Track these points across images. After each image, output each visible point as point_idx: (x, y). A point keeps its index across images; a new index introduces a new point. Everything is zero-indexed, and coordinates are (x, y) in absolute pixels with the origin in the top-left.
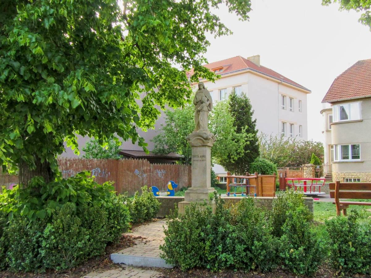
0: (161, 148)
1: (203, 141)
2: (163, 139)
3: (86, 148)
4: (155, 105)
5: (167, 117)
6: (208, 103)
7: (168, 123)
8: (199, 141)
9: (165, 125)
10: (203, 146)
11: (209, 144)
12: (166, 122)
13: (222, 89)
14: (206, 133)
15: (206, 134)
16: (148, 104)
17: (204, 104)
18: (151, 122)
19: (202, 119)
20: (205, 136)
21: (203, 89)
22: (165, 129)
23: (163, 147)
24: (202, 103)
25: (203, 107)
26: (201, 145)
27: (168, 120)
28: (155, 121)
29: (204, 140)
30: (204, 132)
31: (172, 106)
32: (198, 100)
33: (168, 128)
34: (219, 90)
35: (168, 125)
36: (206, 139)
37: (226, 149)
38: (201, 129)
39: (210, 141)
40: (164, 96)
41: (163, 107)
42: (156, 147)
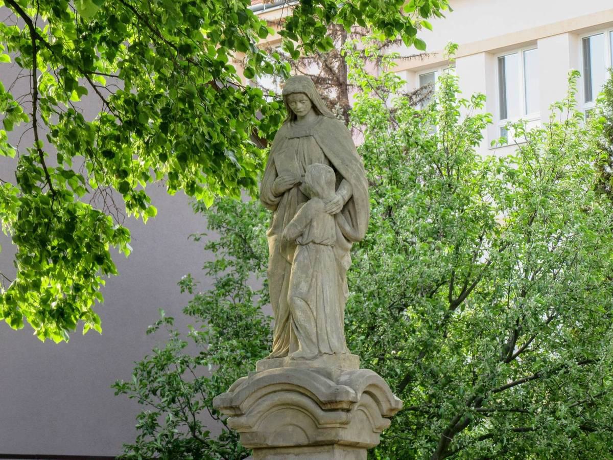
0: (182, 432)
1: (316, 422)
2: (188, 378)
3: (427, 58)
4: (90, 192)
5: (215, 236)
6: (339, 197)
7: (222, 274)
8: (289, 416)
9: (206, 286)
10: (317, 444)
11: (347, 435)
12: (215, 267)
13: (597, 29)
14: (333, 369)
15: (329, 376)
16: (45, 192)
17: (314, 203)
18: (77, 288)
19: (304, 287)
20: (322, 388)
21: (312, 117)
22: (204, 309)
23: (193, 428)
24: (307, 198)
25: (310, 224)
26: (303, 440)
27: (222, 254)
28: (100, 279)
29: (319, 412)
30: (317, 364)
31: (192, 188)
32: (286, 181)
33: (225, 303)
34: (575, 33)
35: (225, 285)
36: (331, 405)
37: (587, 427)
38: (302, 348)
39: (357, 414)
40: (140, 134)
41: (139, 201)
42: (152, 426)
